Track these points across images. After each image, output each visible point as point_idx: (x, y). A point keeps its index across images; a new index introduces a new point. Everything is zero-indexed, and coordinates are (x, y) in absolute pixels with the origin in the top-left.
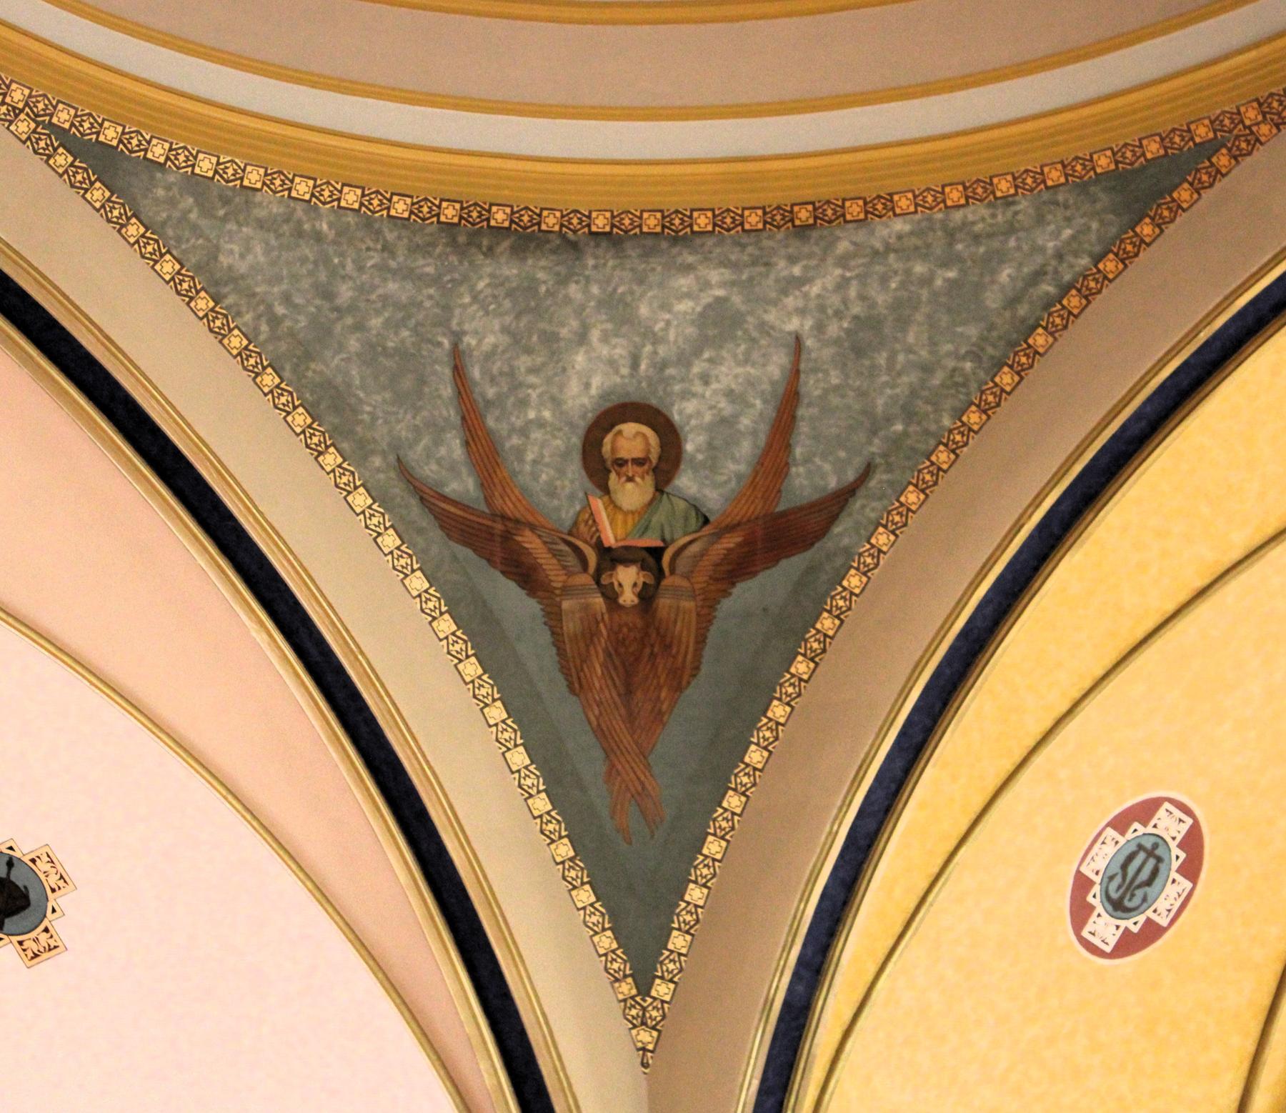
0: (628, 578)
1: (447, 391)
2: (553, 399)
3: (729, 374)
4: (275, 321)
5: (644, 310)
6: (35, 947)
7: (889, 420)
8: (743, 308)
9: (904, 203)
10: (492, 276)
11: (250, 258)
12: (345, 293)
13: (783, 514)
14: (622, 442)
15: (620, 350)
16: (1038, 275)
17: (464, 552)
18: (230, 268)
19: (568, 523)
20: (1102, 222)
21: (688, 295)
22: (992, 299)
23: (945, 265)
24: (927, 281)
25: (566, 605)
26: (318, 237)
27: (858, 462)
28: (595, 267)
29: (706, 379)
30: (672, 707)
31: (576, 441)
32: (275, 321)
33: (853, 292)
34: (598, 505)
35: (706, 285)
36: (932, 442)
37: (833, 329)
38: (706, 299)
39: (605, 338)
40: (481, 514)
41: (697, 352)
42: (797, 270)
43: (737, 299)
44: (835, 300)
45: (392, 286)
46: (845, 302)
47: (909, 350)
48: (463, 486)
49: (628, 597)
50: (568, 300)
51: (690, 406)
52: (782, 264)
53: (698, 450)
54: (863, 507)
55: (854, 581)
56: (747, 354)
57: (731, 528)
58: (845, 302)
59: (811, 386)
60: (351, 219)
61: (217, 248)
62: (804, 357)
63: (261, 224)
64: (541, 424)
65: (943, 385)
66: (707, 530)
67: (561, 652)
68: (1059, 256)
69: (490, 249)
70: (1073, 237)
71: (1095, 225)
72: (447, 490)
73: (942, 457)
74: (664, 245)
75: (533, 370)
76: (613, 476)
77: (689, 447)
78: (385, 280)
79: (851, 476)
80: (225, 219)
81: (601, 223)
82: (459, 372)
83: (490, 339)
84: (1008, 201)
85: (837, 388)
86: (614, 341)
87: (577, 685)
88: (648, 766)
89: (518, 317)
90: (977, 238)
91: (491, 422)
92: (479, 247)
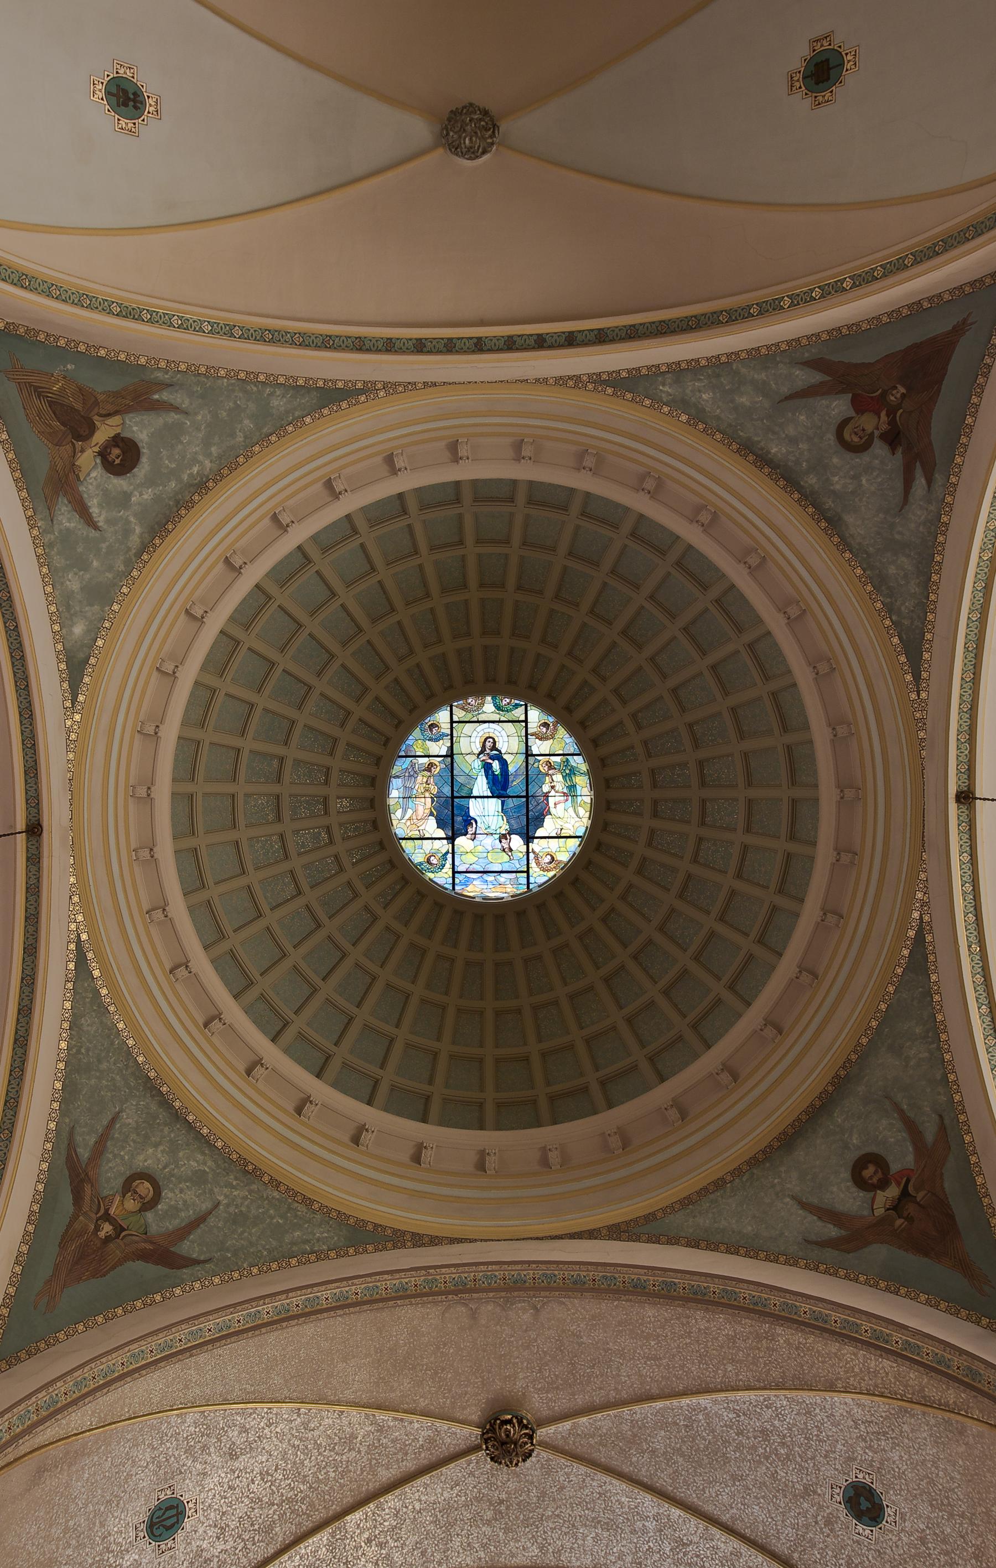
0: (107, 1228)
1: (105, 1123)
2: (132, 1155)
3: (190, 1196)
4: (79, 1052)
5: (181, 1154)
7: (228, 1250)
8: (210, 1180)
9: (282, 1188)
10: (147, 1103)
11: (89, 1028)
13: (174, 1253)
14: (141, 1186)
15: (164, 1159)
16: (307, 1241)
17: (66, 1172)
18: (82, 1025)
19: (104, 1195)
20: (339, 1239)
21: (197, 1162)
22: (287, 1239)
23: (281, 1217)
24: (272, 1218)
25: (81, 1218)
26: (112, 1043)
27: (207, 1256)
28: (178, 1129)
29: (181, 1191)
30: (88, 1279)
31: (128, 1173)
32: (79, 1052)
33: (246, 1203)
34: (118, 1198)
35: (205, 1164)
36: (236, 1268)
37: (232, 1209)
38: (201, 1168)
39: (163, 1152)
40: (81, 1167)
41: (186, 1181)
42: (234, 1183)
43: (210, 1176)
45: (118, 1078)
46: (242, 1204)
47: (250, 1234)
48: (84, 1154)
49: (102, 1234)
50: (162, 1131)
51: (170, 1195)
52: (232, 1177)
53: (162, 1210)
54: (199, 1270)
55: (178, 1291)
56: (200, 1194)
57: (151, 1243)
58: (242, 1204)
59: (211, 1221)
60: (125, 1048)
61: (85, 1016)
62: (216, 1210)
63: (101, 1023)
64: (122, 1158)
65: (253, 1253)
66: (144, 1236)
67: (67, 1231)
68: (318, 1240)
69: (154, 1095)
70: (326, 1237)
71: (336, 1238)
72: (78, 1150)
73: (236, 1275)
74: (203, 1141)
75: (134, 1141)
76: (130, 1194)
77: (159, 1207)
78: (118, 1074)
79: (202, 1258)
80: (94, 1010)
81: (191, 1118)
82: (113, 1121)
83: (130, 1121)
84: (314, 1212)
85: (218, 1227)
86: (165, 1155)
87: (63, 1245)
88: (62, 1292)
89: (144, 1122)
90: (296, 1216)
91: (109, 1143)
92: (151, 1092)
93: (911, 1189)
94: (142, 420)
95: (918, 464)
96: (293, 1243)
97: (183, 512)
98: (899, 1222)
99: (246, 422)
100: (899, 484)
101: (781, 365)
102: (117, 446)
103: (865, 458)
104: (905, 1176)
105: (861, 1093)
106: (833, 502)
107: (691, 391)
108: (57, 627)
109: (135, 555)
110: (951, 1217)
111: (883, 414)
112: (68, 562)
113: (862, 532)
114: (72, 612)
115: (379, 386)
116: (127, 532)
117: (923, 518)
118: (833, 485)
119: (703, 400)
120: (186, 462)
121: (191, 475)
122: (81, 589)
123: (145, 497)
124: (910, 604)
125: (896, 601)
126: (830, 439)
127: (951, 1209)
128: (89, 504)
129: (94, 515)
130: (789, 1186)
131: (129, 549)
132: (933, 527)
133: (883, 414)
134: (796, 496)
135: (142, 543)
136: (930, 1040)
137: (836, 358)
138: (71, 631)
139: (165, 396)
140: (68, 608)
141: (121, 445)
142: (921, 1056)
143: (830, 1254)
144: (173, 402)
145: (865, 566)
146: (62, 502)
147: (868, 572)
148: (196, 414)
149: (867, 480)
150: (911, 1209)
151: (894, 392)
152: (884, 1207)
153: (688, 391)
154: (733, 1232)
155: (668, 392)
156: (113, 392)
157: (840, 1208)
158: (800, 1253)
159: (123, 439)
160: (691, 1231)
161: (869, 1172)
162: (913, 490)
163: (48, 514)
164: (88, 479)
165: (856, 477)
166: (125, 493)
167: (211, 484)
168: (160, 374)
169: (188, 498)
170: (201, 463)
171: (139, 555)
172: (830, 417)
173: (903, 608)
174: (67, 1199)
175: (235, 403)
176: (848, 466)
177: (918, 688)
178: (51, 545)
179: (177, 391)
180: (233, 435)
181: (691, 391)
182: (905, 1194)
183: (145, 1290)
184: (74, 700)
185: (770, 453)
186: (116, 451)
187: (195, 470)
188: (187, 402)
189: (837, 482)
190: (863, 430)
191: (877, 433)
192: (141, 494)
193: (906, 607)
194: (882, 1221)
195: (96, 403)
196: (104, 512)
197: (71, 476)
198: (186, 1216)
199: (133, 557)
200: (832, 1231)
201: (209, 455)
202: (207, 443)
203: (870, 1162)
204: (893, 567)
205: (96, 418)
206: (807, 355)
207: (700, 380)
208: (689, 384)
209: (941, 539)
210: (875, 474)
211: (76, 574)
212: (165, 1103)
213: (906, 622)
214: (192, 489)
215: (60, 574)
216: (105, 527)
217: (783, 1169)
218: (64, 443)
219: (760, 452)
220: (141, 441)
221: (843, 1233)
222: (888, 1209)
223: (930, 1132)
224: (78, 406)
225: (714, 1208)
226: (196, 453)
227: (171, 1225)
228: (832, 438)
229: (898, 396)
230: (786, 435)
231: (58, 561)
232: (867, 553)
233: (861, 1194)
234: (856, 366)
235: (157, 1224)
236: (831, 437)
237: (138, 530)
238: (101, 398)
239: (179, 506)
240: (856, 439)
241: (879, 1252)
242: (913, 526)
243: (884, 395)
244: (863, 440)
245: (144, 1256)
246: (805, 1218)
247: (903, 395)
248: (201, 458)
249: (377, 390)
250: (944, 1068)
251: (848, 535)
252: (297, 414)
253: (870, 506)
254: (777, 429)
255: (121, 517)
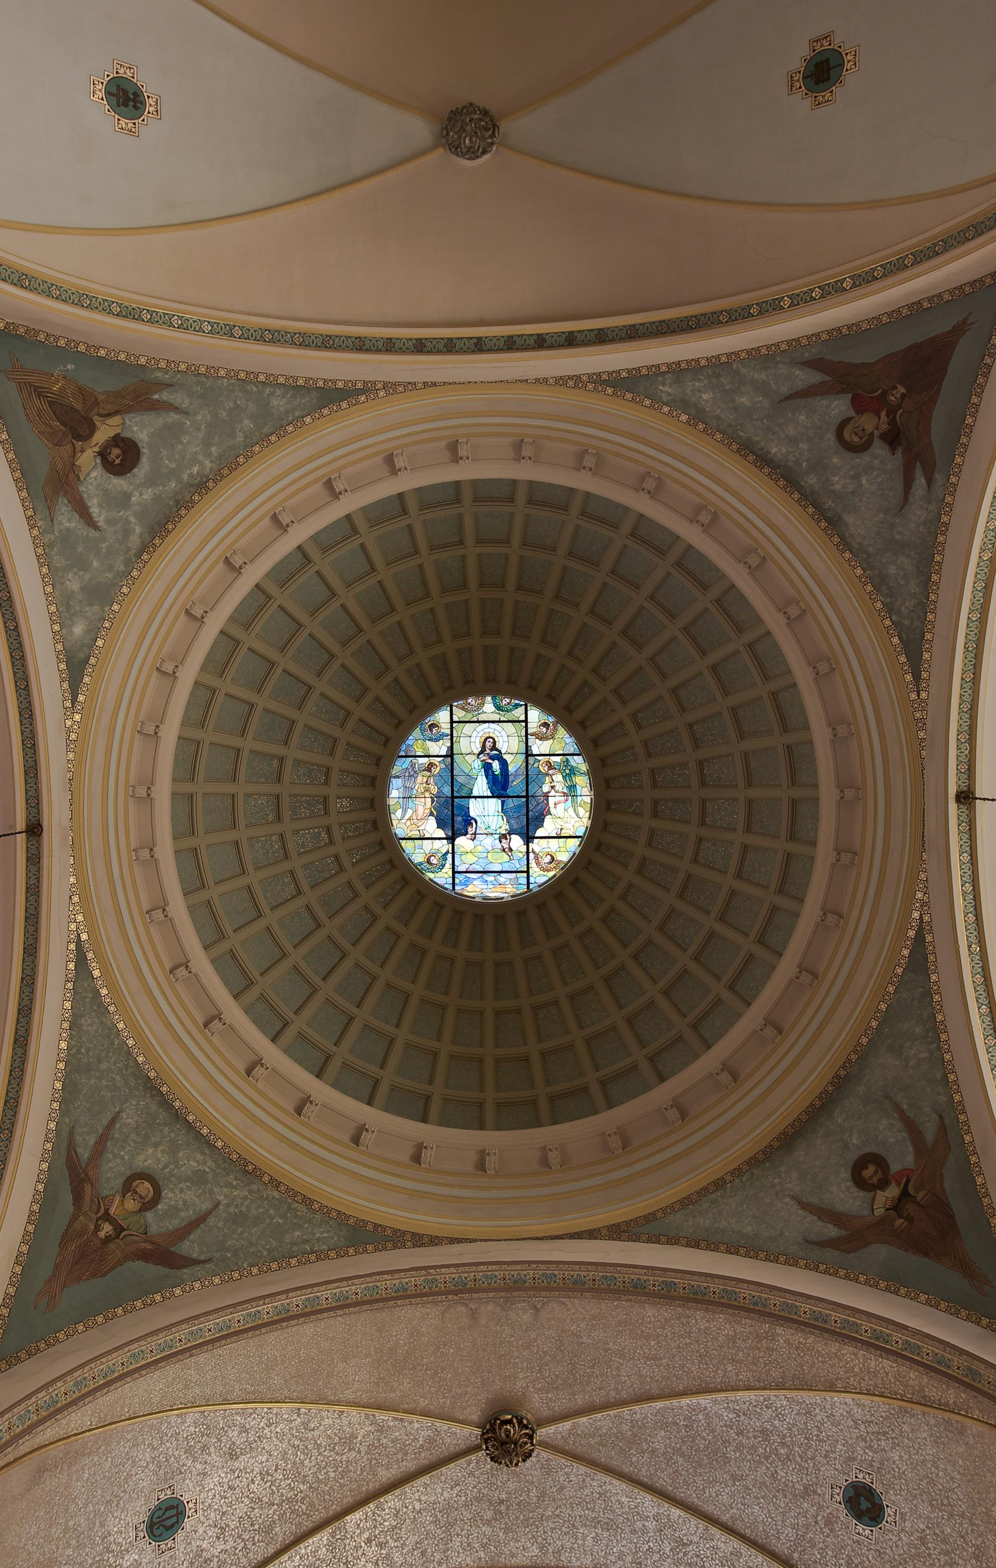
0: (107, 1228)
1: (105, 1123)
2: (132, 1155)
3: (190, 1196)
4: (79, 1052)
5: (181, 1154)
6: (795, 79)
7: (228, 1250)
8: (210, 1180)
9: (282, 1188)
10: (147, 1103)
11: (89, 1028)
12: (104, 1066)
13: (174, 1253)
14: (141, 1186)
15: (164, 1159)
16: (307, 1241)
17: (66, 1172)
18: (82, 1025)
19: (104, 1195)
20: (339, 1239)
21: (197, 1162)
22: (287, 1239)
23: (281, 1217)
24: (272, 1218)
25: (81, 1218)
26: (112, 1043)
27: (207, 1256)
28: (178, 1129)
29: (181, 1191)
30: (88, 1279)
31: (128, 1173)
33: (246, 1203)
34: (118, 1198)
35: (205, 1164)
36: (236, 1268)
37: (232, 1209)
38: (201, 1168)
39: (163, 1152)
40: (81, 1167)
41: (186, 1181)
42: (234, 1183)
43: (210, 1176)
44: (239, 1201)
45: (118, 1078)
46: (242, 1204)
47: (250, 1234)
48: (84, 1154)
49: (102, 1234)
50: (162, 1131)
51: (170, 1195)
52: (232, 1177)
53: (162, 1210)
54: (199, 1270)
55: (178, 1291)
56: (200, 1194)
57: (151, 1243)
58: (242, 1204)
59: (211, 1221)
60: (125, 1048)
61: (85, 1016)
62: (216, 1210)
63: (101, 1023)
64: (122, 1158)
65: (253, 1253)
66: (144, 1236)
67: (67, 1231)
68: (318, 1240)
69: (154, 1095)
70: (326, 1237)
71: (336, 1238)
72: (78, 1150)
73: (236, 1275)
74: (203, 1141)
75: (134, 1141)
76: (130, 1194)
77: (159, 1207)
78: (118, 1074)
79: (202, 1258)
80: (94, 1010)
81: (191, 1118)
82: (113, 1121)
83: (130, 1121)
84: (314, 1212)
85: (218, 1227)
86: (165, 1155)
87: (63, 1245)
88: (62, 1292)
89: (144, 1122)
90: (296, 1216)
91: (109, 1143)
92: (151, 1092)
93: (911, 1189)
94: (142, 420)
95: (918, 464)
96: (293, 1243)
97: (183, 512)
98: (899, 1222)
99: (246, 422)
100: (899, 484)
101: (781, 365)
102: (117, 446)
103: (865, 458)
104: (905, 1176)
105: (861, 1093)
106: (833, 502)
107: (691, 391)
108: (57, 627)
109: (135, 555)
110: (951, 1217)
111: (883, 414)
112: (68, 562)
113: (862, 532)
114: (72, 612)
115: (379, 386)
116: (127, 532)
117: (923, 518)
118: (833, 485)
119: (703, 400)
120: (186, 462)
121: (191, 475)
122: (81, 589)
123: (145, 497)
124: (910, 604)
125: (896, 601)
126: (830, 439)
127: (951, 1209)
128: (89, 504)
129: (94, 515)
130: (789, 1186)
131: (129, 549)
132: (933, 527)
133: (883, 414)
134: (796, 496)
135: (142, 543)
136: (930, 1040)
137: (836, 358)
138: (71, 631)
139: (165, 396)
140: (68, 608)
141: (121, 445)
142: (921, 1056)
143: (830, 1254)
144: (173, 402)
145: (865, 566)
146: (62, 502)
147: (868, 572)
148: (196, 414)
149: (867, 480)
150: (911, 1209)
151: (894, 392)
152: (884, 1207)
153: (688, 391)
154: (733, 1232)
155: (668, 392)
156: (113, 392)
157: (840, 1208)
158: (800, 1253)
159: (123, 439)
160: (691, 1231)
161: (869, 1172)
162: (913, 490)
163: (48, 514)
164: (88, 479)
165: (856, 477)
166: (125, 493)
167: (211, 484)
168: (160, 374)
169: (188, 498)
170: (201, 463)
171: (139, 555)
172: (830, 417)
173: (903, 608)
174: (67, 1199)
175: (235, 403)
176: (848, 466)
177: (918, 688)
178: (51, 545)
179: (177, 391)
180: (233, 435)
181: (691, 391)
182: (905, 1194)
183: (145, 1290)
184: (74, 700)
185: (770, 453)
186: (116, 451)
187: (195, 470)
188: (187, 402)
189: (837, 482)
190: (863, 430)
191: (877, 433)
192: (141, 494)
193: (906, 607)
194: (882, 1221)
195: (96, 403)
196: (104, 512)
197: (71, 476)
198: (186, 1216)
199: (133, 557)
200: (832, 1231)
201: (209, 455)
202: (207, 443)
203: (870, 1162)
204: (893, 567)
205: (96, 418)
206: (807, 355)
207: (700, 380)
208: (689, 384)
209: (941, 539)
210: (875, 474)
211: (76, 574)
212: (165, 1103)
213: (906, 622)
214: (192, 489)
215: (60, 574)
216: (105, 527)
217: (783, 1169)
218: (64, 443)
219: (760, 452)
220: (141, 441)
221: (843, 1233)
222: (888, 1209)
223: (930, 1132)
224: (78, 406)
225: (714, 1208)
226: (196, 453)
227: (171, 1225)
228: (832, 438)
229: (898, 396)
230: (786, 435)
231: (58, 561)
232: (867, 553)
233: (861, 1194)
234: (856, 366)
235: (157, 1224)
236: (831, 437)
237: (138, 530)
238: (101, 398)
239: (179, 506)
240: (856, 439)
241: (879, 1252)
242: (913, 526)
243: (884, 395)
244: (863, 440)
245: (144, 1256)
246: (805, 1218)
247: (903, 395)
248: (201, 458)
249: (377, 390)
250: (944, 1068)
251: (848, 535)
252: (297, 414)
253: (870, 506)
254: (777, 429)
255: (121, 517)
